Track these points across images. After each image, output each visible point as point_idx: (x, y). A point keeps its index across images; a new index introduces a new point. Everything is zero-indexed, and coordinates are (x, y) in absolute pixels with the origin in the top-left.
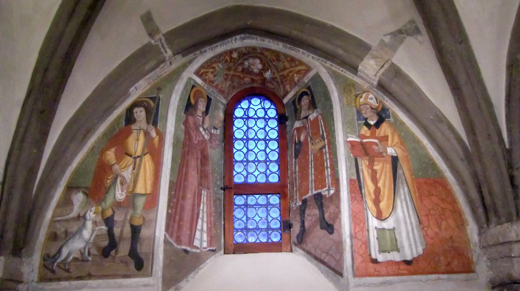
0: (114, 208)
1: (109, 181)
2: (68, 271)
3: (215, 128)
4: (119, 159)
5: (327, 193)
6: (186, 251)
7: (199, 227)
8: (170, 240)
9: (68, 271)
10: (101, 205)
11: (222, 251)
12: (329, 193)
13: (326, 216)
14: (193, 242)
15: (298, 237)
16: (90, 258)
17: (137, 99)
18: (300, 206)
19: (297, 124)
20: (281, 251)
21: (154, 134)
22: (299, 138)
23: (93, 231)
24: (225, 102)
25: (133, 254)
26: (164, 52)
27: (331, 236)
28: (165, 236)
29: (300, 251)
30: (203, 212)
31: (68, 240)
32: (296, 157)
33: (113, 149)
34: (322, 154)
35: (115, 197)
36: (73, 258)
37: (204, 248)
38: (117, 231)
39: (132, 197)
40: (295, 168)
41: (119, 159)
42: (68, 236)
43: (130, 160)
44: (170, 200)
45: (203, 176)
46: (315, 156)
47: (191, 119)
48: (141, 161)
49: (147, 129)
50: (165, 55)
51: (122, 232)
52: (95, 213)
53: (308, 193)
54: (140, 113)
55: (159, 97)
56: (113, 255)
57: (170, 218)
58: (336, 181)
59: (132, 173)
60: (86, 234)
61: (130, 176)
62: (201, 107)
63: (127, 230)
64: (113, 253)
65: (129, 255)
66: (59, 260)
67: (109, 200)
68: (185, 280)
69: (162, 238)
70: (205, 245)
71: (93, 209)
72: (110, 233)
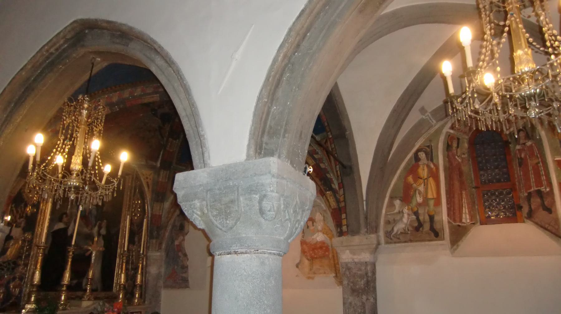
0: (417, 206)
1: (412, 193)
2: (399, 239)
3: (464, 154)
4: (415, 181)
5: (544, 190)
6: (459, 226)
7: (464, 212)
8: (451, 221)
9: (399, 239)
10: (410, 205)
11: (479, 223)
12: (546, 190)
13: (546, 203)
14: (462, 220)
15: (528, 214)
16: (409, 232)
17: (419, 147)
18: (527, 196)
19: (518, 147)
20: (517, 222)
21: (432, 166)
22: (521, 155)
23: (408, 218)
24: (467, 137)
25: (432, 229)
26: (432, 122)
27: (551, 215)
28: (448, 219)
29: (530, 222)
30: (465, 203)
31: (396, 223)
32: (520, 166)
33: (411, 176)
34: (538, 167)
35: (417, 201)
36: (400, 232)
37: (468, 223)
38: (421, 218)
39: (426, 201)
40: (520, 173)
41: (415, 181)
42: (395, 222)
43: (422, 181)
44: (447, 201)
45: (462, 183)
46: (533, 167)
47: (450, 154)
48: (428, 181)
49: (428, 164)
50: (432, 123)
51: (424, 218)
52: (407, 210)
53: (531, 189)
54: (422, 155)
55: (432, 146)
56: (421, 230)
57: (449, 209)
58: (550, 184)
59: (424, 188)
60: (405, 220)
61: (423, 190)
62: (455, 145)
63: (427, 218)
64: (421, 229)
65: (430, 230)
66: (393, 234)
67: (414, 203)
68: (461, 241)
69: (447, 221)
70: (468, 221)
71: (406, 208)
72: (418, 219)
